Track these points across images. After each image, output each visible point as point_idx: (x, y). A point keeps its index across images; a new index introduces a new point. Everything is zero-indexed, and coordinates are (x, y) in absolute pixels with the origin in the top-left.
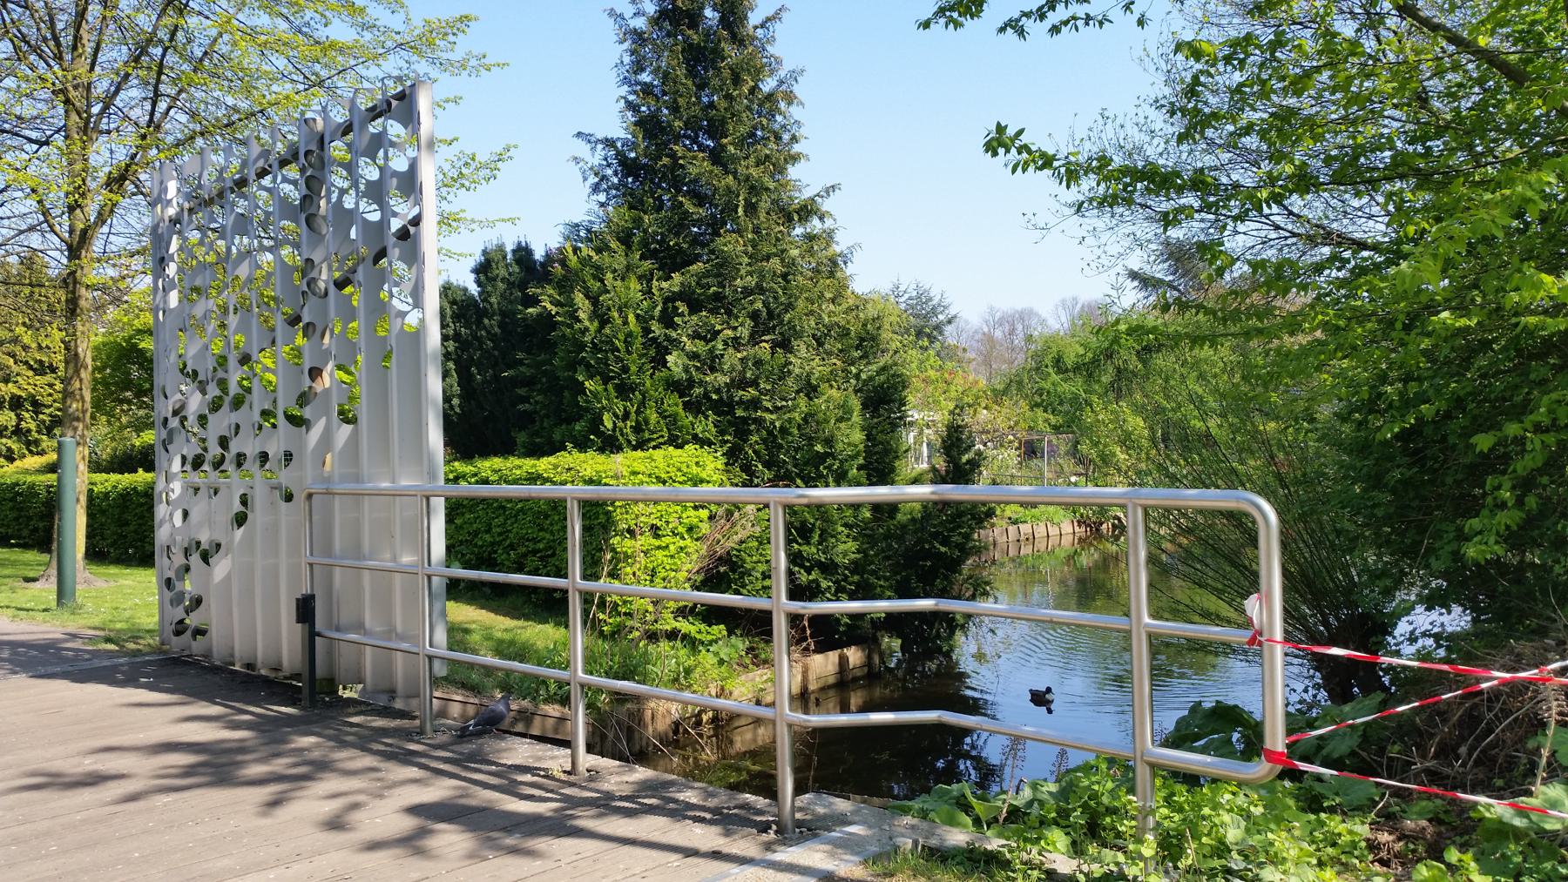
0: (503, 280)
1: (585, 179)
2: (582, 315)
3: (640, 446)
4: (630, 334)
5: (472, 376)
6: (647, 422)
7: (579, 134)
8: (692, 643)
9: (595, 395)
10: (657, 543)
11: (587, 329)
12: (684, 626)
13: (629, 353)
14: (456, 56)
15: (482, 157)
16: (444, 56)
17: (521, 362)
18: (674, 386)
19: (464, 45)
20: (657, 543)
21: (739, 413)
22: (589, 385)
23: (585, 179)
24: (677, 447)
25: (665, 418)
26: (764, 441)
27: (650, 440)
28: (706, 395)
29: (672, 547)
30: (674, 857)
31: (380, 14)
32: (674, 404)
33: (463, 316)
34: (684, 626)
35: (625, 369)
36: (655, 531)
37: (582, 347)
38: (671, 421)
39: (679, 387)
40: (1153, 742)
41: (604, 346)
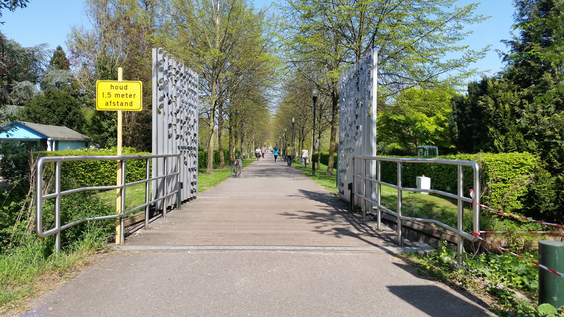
0: (474, 94)
1: (500, 57)
2: (490, 105)
3: (506, 151)
4: (505, 112)
5: (462, 126)
6: (508, 143)
7: (502, 41)
8: (519, 223)
9: (493, 133)
10: (504, 185)
11: (491, 110)
12: (516, 216)
13: (505, 118)
14: (473, 17)
15: (480, 50)
16: (468, 18)
17: (474, 122)
18: (519, 130)
19: (475, 13)
20: (504, 185)
21: (546, 140)
22: (491, 129)
23: (500, 57)
24: (519, 152)
25: (516, 141)
26: (558, 151)
27: (509, 149)
28: (534, 133)
29: (510, 187)
30: (366, 243)
31: (444, 9)
32: (519, 136)
33: (460, 106)
34: (516, 216)
35: (503, 124)
36: (504, 181)
37: (490, 116)
38: (518, 142)
39: (524, 131)
40: (463, 229)
41: (497, 115)
